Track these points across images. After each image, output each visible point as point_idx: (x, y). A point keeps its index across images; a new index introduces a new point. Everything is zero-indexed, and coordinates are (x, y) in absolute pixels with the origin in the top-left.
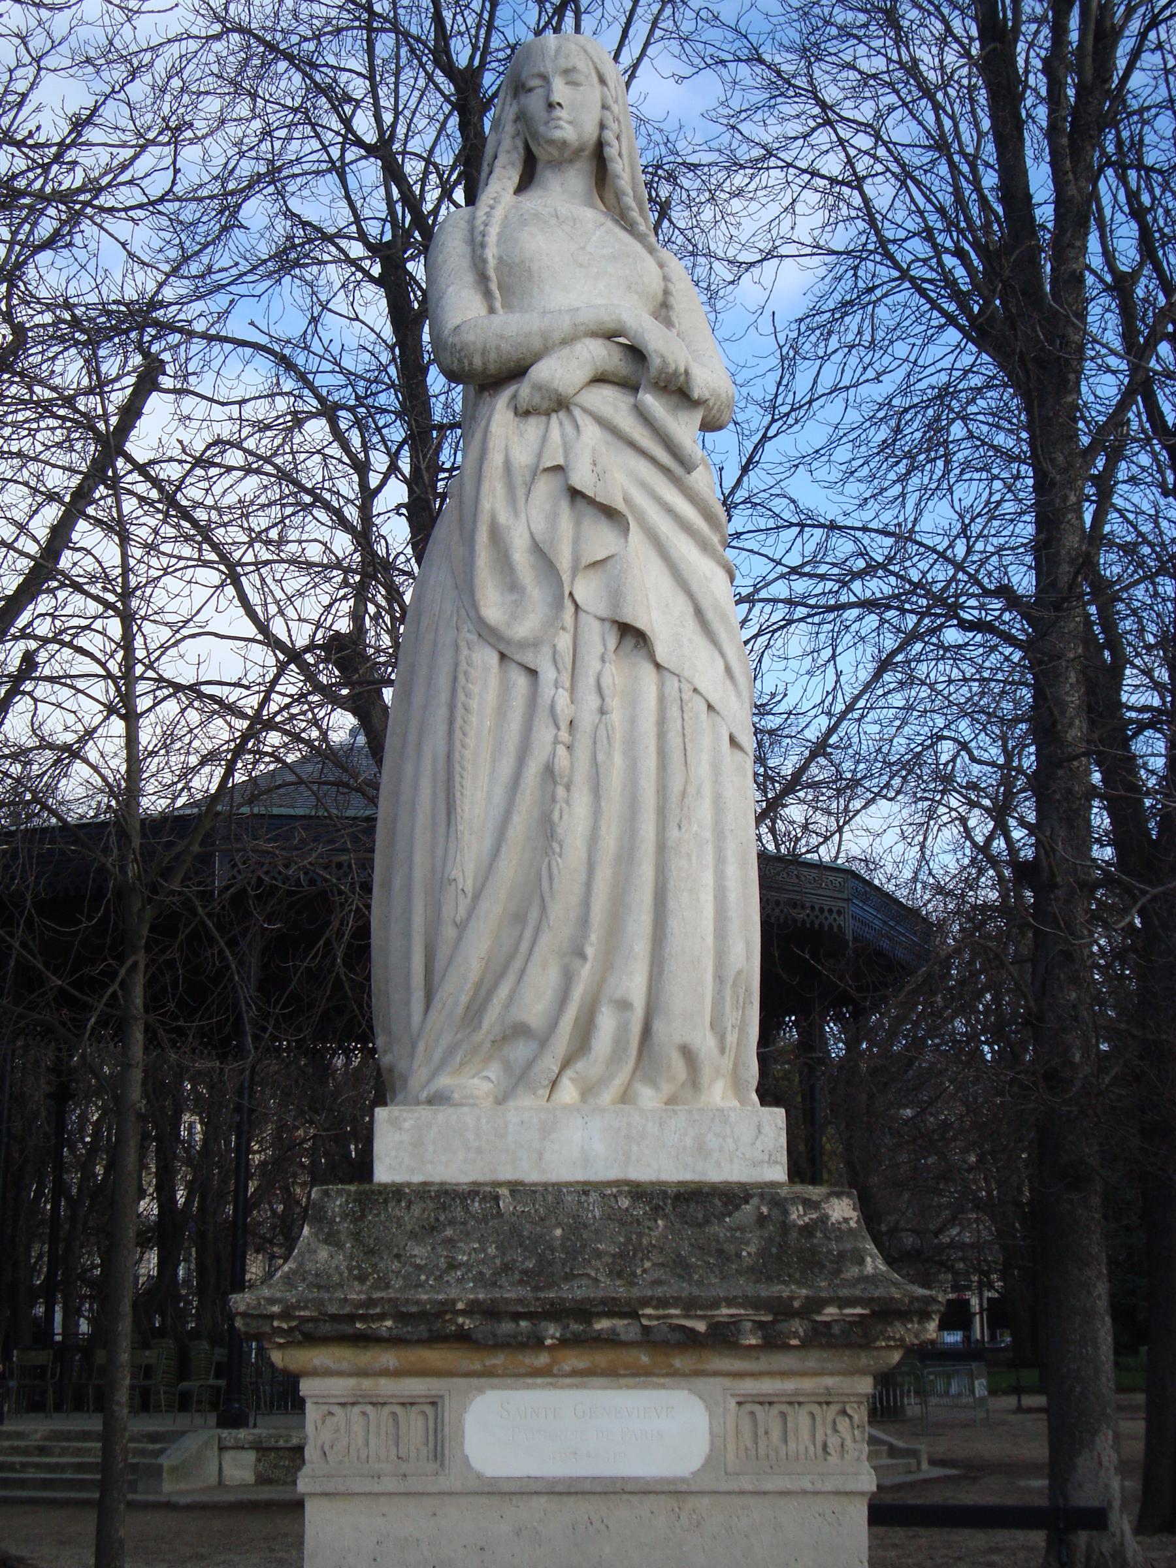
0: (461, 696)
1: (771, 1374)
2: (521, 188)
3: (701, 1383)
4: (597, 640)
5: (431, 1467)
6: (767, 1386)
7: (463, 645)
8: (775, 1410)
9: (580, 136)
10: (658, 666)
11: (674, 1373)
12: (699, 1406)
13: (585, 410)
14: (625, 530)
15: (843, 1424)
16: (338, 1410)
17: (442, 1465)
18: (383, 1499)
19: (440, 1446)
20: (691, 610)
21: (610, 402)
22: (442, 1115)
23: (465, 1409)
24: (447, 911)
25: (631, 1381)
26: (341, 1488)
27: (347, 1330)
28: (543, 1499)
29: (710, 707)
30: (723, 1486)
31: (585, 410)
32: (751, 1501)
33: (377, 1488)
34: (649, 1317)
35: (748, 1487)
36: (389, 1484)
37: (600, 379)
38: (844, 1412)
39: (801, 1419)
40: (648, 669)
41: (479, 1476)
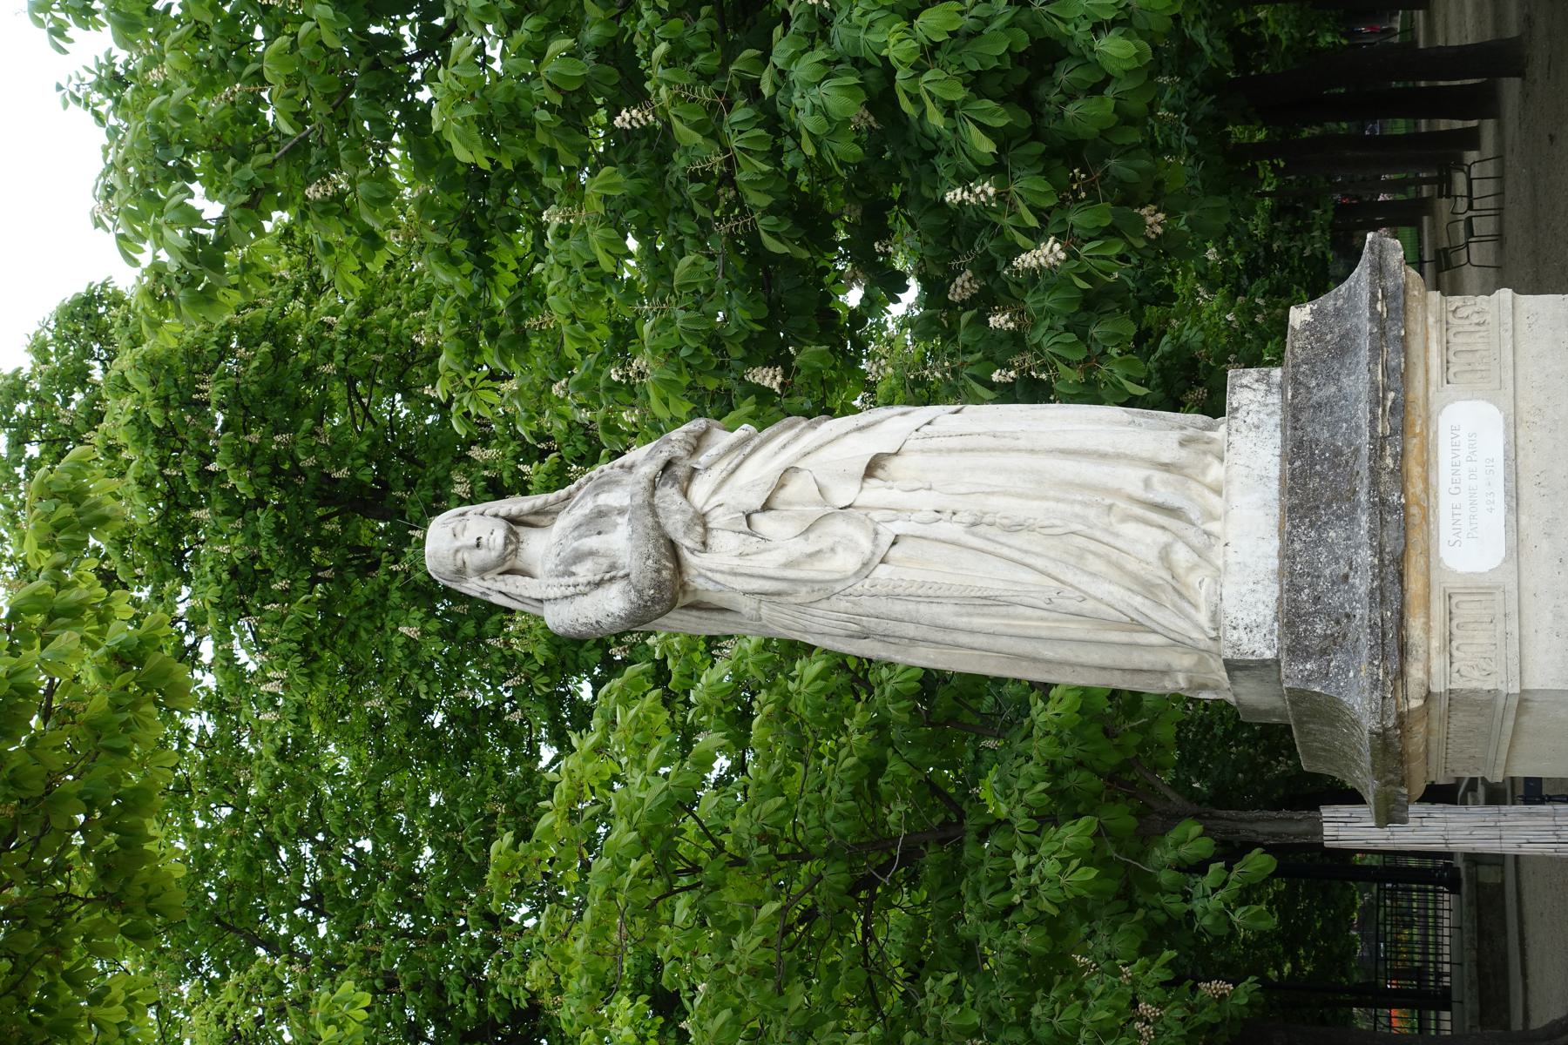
0: (912, 590)
1: (1426, 349)
3: (1434, 408)
4: (874, 493)
5: (1499, 596)
6: (1435, 361)
7: (873, 591)
8: (1452, 359)
9: (601, 22)
10: (896, 454)
11: (1426, 518)
12: (1445, 411)
14: (797, 470)
15: (1464, 312)
16: (1456, 666)
17: (1497, 588)
19: (1482, 589)
20: (856, 434)
21: (700, 490)
22: (1231, 608)
24: (1074, 606)
27: (1394, 647)
28: (1524, 519)
32: (1520, 372)
34: (1384, 428)
35: (1511, 374)
36: (1513, 626)
37: (685, 494)
39: (1458, 342)
40: (896, 461)
41: (1505, 561)
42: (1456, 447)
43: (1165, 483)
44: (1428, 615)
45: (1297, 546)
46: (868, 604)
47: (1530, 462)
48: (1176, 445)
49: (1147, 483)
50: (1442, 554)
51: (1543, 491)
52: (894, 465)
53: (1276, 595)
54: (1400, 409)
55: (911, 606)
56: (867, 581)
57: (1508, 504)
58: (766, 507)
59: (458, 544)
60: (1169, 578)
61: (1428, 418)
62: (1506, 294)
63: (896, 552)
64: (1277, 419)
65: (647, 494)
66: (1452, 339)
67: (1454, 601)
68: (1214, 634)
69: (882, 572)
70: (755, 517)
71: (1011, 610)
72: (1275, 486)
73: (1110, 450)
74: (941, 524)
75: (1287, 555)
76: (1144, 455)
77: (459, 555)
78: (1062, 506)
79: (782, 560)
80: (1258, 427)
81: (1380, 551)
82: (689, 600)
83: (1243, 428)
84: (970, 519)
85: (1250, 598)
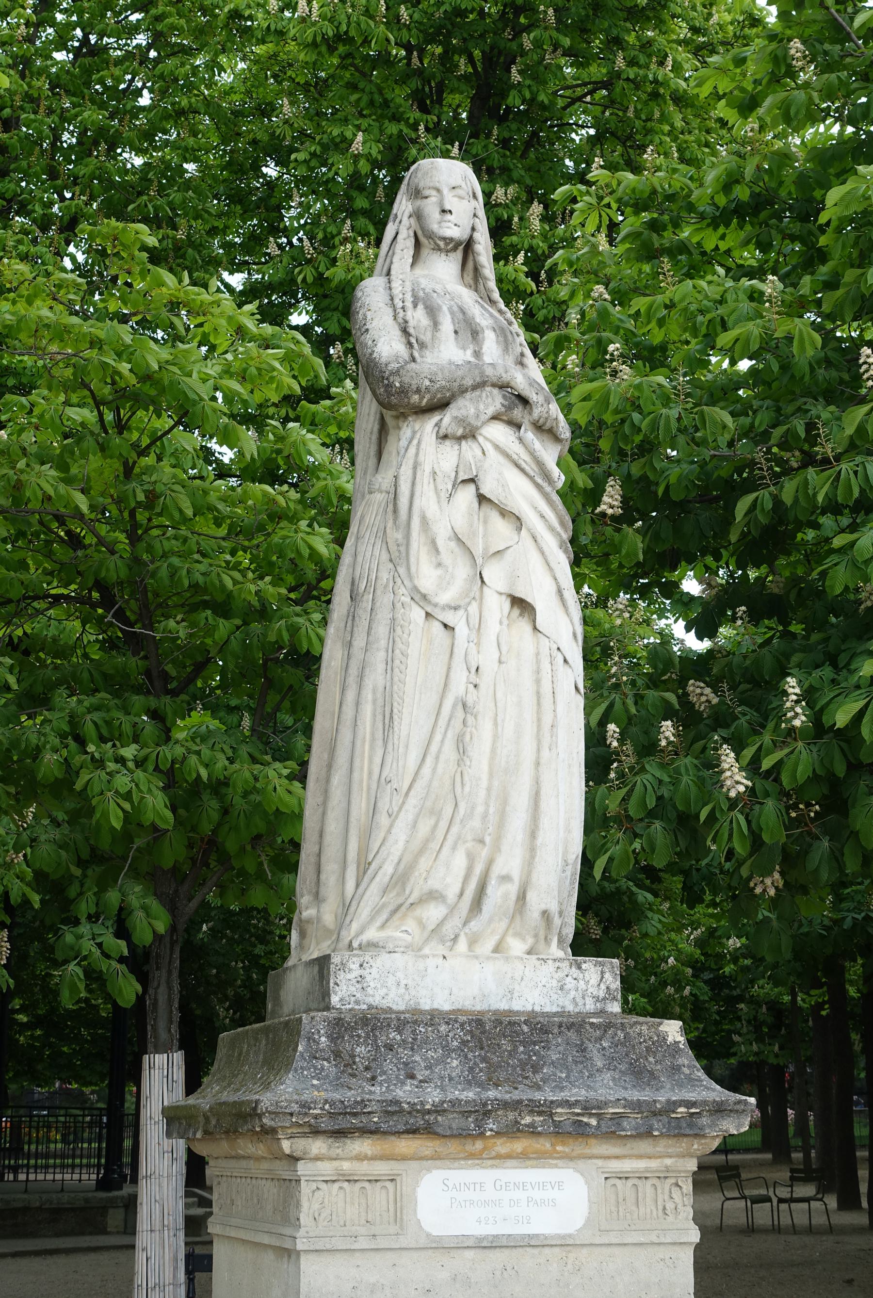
0: (399, 645)
1: (640, 1157)
2: (413, 265)
3: (581, 1164)
4: (496, 607)
5: (393, 1229)
6: (627, 1165)
7: (399, 605)
8: (630, 1183)
10: (535, 628)
11: (471, 1156)
12: (578, 1176)
13: (486, 438)
14: (519, 529)
16: (323, 1186)
18: (357, 1254)
19: (400, 1212)
20: (554, 588)
21: (499, 432)
22: (381, 962)
23: (417, 1183)
25: (535, 1162)
26: (328, 1247)
27: (343, 1124)
28: (469, 1254)
29: (565, 661)
30: (597, 1241)
31: (486, 438)
32: (616, 1251)
33: (356, 1246)
34: (561, 1114)
36: (362, 1243)
37: (495, 418)
38: (677, 1185)
39: (647, 1188)
40: (528, 628)
41: (428, 1235)
42: (542, 1186)
43: (506, 896)
44: (373, 1158)
45: (443, 1028)
46: (385, 600)
47: (527, 1259)
48: (543, 907)
49: (506, 878)
50: (435, 1172)
51: (498, 1273)
52: (524, 626)
53: (394, 1007)
54: (580, 1131)
55: (383, 643)
56: (407, 599)
57: (486, 1237)
58: (482, 499)
59: (445, 191)
60: (411, 901)
61: (571, 1159)
62: (695, 1236)
63: (437, 627)
64: (570, 1008)
65: (495, 380)
66: (649, 1183)
67: (389, 1185)
68: (355, 944)
69: (417, 614)
70: (472, 488)
71: (380, 743)
72: (503, 1006)
73: (539, 841)
74: (466, 673)
75: (434, 1018)
76: (534, 876)
77: (434, 193)
78: (482, 793)
79: (429, 515)
80: (562, 989)
81: (438, 1110)
82: (390, 421)
83: (561, 974)
84: (470, 702)
85: (391, 980)
